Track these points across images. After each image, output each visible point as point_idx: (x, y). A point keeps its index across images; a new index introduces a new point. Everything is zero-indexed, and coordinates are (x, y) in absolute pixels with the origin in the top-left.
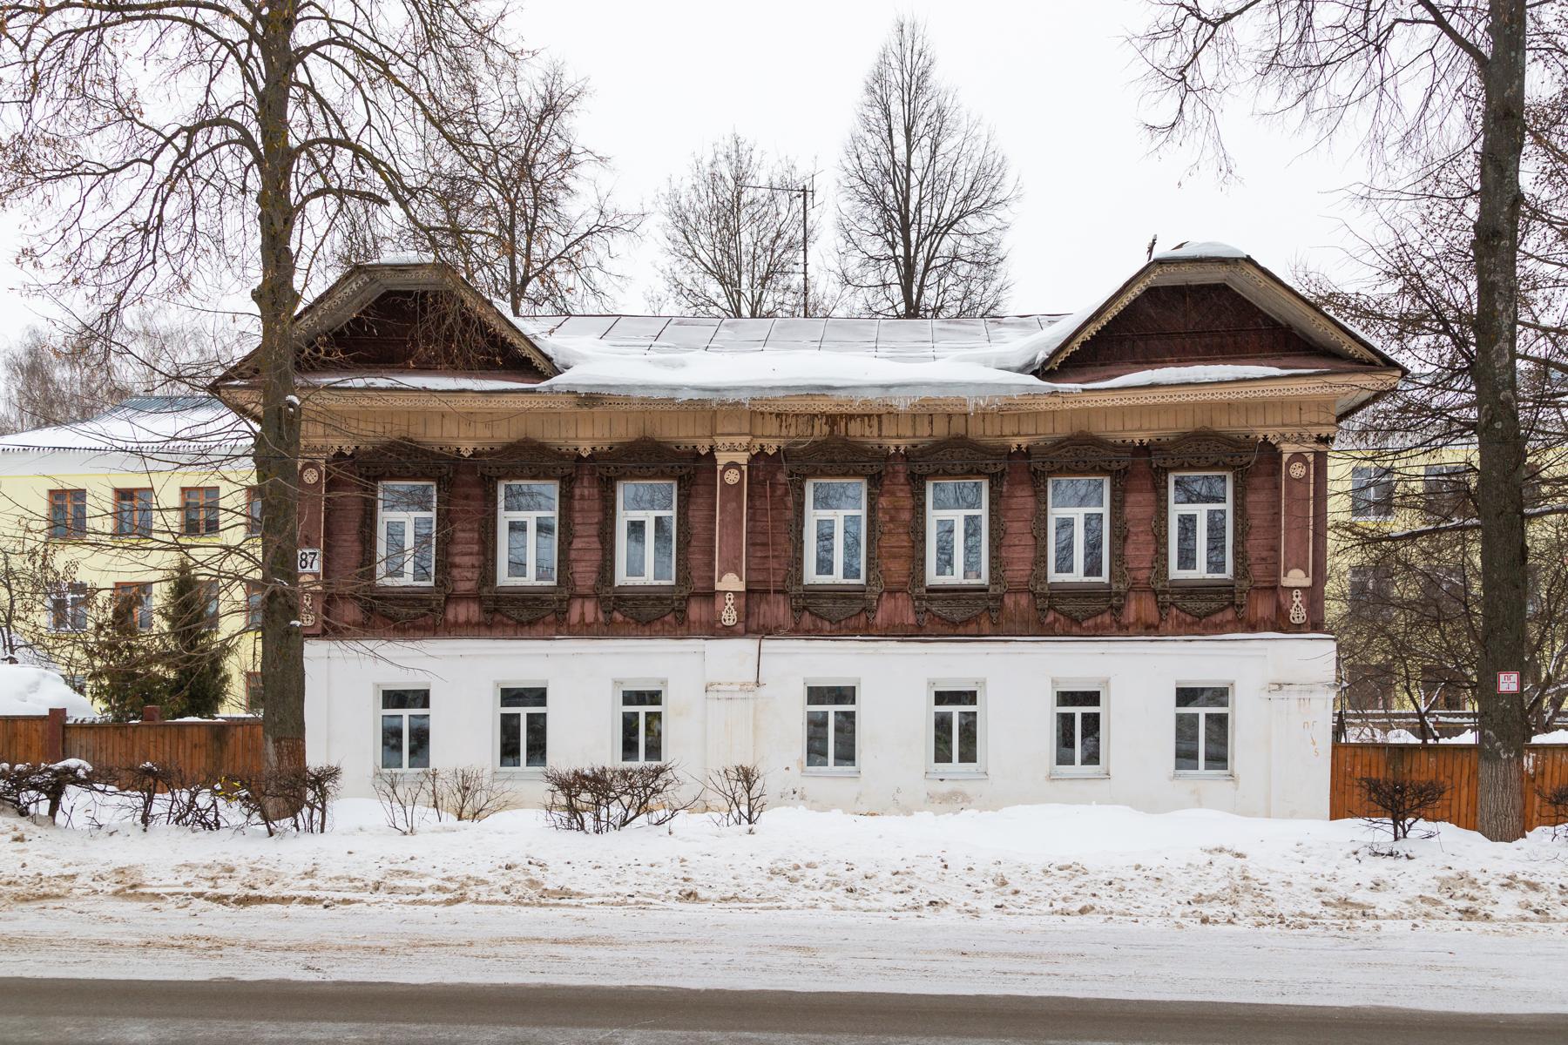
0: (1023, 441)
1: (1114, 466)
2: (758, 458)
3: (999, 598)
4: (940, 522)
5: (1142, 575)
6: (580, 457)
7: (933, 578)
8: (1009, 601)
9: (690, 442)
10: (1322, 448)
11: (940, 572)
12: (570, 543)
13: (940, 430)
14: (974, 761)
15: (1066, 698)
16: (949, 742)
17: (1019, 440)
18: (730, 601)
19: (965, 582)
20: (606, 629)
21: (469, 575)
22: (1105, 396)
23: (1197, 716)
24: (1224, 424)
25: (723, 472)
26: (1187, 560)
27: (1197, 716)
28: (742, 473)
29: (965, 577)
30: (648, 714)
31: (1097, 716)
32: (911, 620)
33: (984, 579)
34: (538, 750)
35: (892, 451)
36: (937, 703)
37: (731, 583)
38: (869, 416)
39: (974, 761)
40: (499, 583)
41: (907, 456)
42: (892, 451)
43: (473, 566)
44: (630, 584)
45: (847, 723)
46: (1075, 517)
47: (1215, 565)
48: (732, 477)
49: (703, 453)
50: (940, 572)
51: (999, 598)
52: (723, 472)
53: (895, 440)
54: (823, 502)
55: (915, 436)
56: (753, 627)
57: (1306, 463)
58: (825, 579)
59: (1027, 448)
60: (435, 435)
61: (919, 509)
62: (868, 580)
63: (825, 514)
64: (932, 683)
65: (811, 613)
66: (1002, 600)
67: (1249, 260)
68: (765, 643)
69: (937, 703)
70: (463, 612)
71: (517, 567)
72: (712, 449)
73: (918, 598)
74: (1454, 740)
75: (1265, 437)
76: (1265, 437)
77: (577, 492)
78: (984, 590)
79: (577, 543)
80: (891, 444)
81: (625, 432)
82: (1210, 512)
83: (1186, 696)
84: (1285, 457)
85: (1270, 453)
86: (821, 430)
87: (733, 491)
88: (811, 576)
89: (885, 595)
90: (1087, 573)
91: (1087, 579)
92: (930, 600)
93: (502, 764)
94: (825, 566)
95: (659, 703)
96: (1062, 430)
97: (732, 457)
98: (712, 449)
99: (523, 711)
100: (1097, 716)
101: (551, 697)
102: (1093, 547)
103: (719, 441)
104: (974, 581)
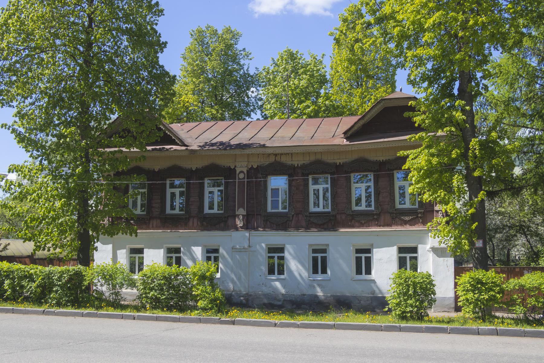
0: (341, 161)
3: (335, 216)
6: (193, 170)
7: (312, 209)
8: (338, 217)
9: (228, 165)
11: (357, 205)
12: (189, 199)
13: (313, 158)
14: (313, 273)
15: (358, 251)
19: (324, 210)
21: (157, 210)
23: (361, 257)
25: (238, 175)
26: (317, 204)
27: (361, 257)
28: (245, 174)
29: (324, 208)
33: (329, 209)
35: (296, 166)
36: (269, 253)
37: (241, 212)
38: (288, 154)
39: (313, 273)
40: (167, 213)
42: (296, 166)
43: (158, 207)
44: (209, 212)
45: (324, 260)
46: (406, 184)
47: (369, 205)
49: (232, 167)
50: (357, 205)
51: (335, 216)
52: (238, 175)
53: (297, 162)
54: (316, 182)
55: (346, 159)
56: (247, 226)
58: (212, 211)
59: (343, 164)
60: (373, 157)
61: (307, 185)
62: (289, 210)
63: (316, 187)
64: (310, 245)
65: (270, 222)
66: (336, 216)
69: (269, 253)
71: (173, 208)
72: (235, 167)
73: (306, 216)
74: (235, 279)
78: (329, 213)
79: (192, 199)
80: (296, 163)
81: (205, 163)
83: (272, 250)
84: (237, 172)
86: (272, 159)
89: (295, 215)
90: (366, 207)
91: (366, 209)
92: (310, 217)
94: (211, 207)
98: (235, 167)
102: (368, 197)
104: (326, 210)
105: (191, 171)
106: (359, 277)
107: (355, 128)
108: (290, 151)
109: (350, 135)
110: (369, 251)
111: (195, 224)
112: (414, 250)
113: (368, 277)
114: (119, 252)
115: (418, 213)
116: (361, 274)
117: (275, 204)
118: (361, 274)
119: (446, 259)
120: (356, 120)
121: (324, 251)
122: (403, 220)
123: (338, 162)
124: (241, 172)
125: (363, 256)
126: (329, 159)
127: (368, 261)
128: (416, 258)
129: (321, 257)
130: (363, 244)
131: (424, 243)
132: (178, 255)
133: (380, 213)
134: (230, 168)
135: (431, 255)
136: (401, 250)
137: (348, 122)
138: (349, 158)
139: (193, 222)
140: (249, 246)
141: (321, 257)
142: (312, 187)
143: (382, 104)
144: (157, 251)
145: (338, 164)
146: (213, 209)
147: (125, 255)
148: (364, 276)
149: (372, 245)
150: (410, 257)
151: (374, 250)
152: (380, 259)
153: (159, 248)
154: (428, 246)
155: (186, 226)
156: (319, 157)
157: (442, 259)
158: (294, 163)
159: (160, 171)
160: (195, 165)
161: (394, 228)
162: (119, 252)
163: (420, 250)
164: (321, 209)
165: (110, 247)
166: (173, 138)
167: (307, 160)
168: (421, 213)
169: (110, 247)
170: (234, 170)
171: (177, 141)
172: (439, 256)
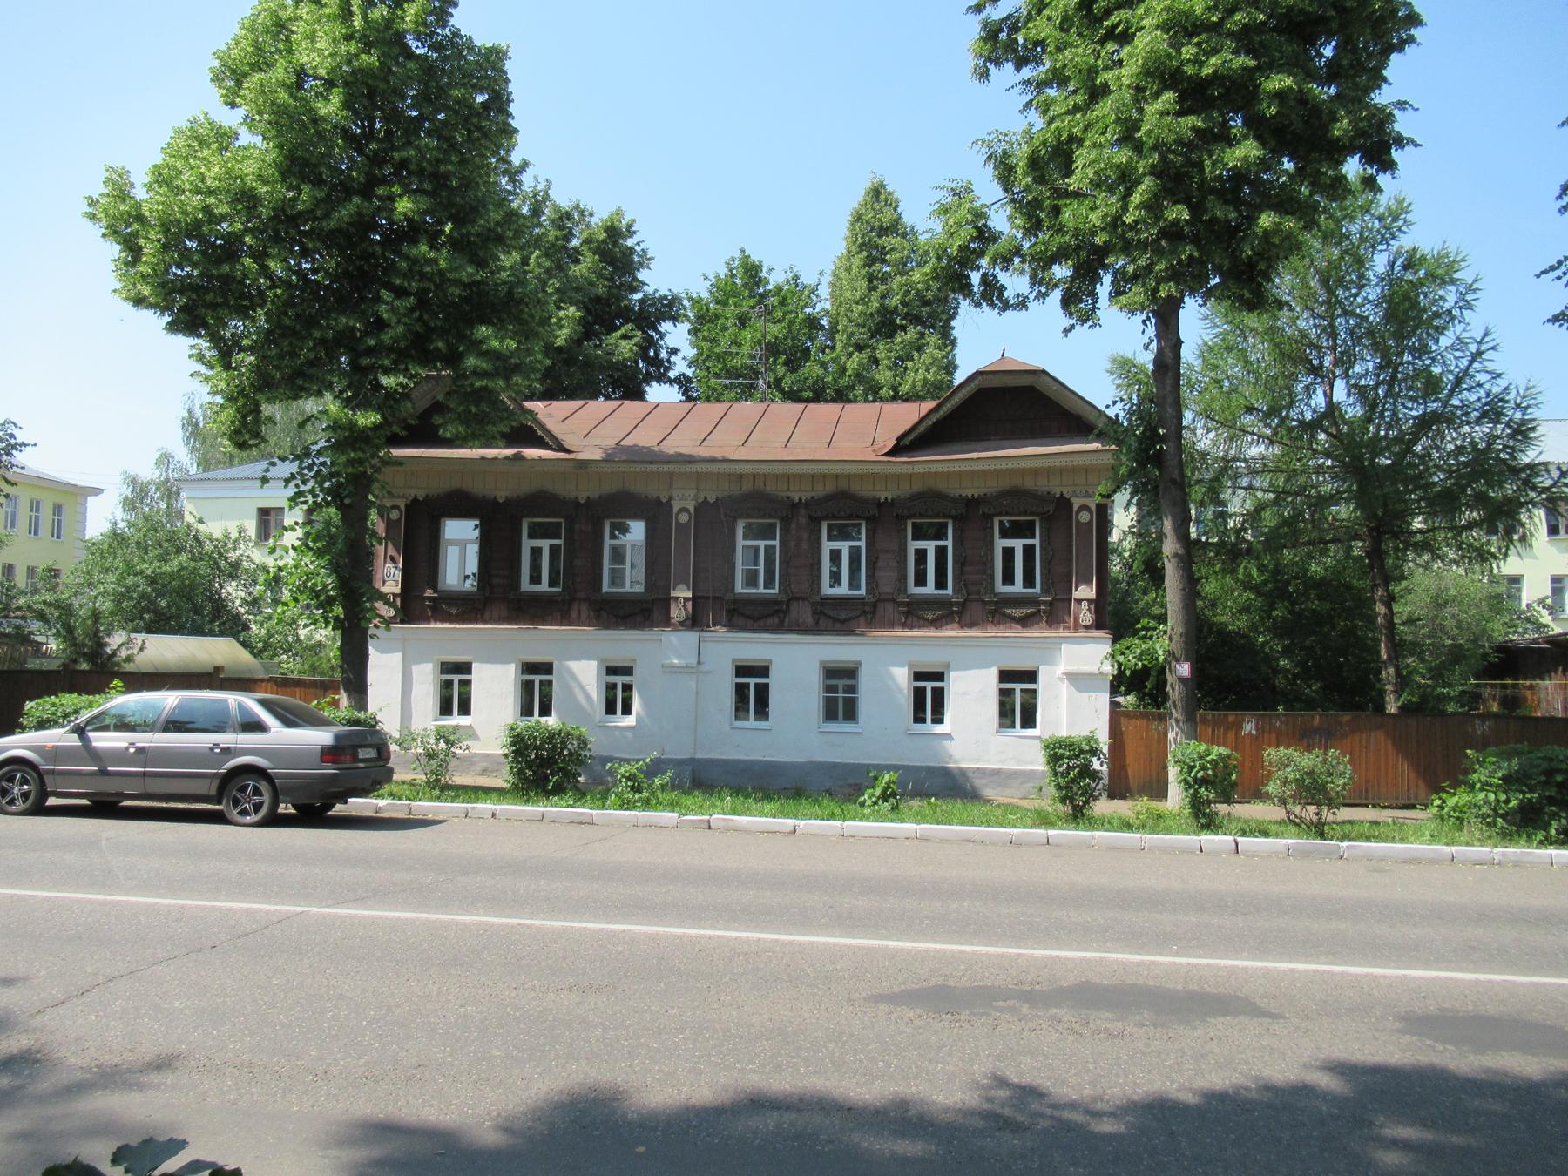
1: (953, 512)
2: (702, 507)
4: (832, 551)
5: (888, 589)
6: (498, 503)
10: (1105, 501)
11: (613, 583)
15: (919, 676)
16: (924, 710)
17: (799, 494)
18: (1084, 607)
20: (815, 629)
22: (906, 466)
23: (925, 688)
24: (1029, 484)
25: (677, 514)
27: (925, 688)
30: (541, 682)
31: (942, 689)
32: (811, 620)
33: (863, 591)
34: (1029, 720)
36: (738, 675)
37: (683, 593)
41: (807, 505)
45: (762, 692)
48: (683, 518)
49: (664, 500)
52: (677, 514)
56: (695, 622)
57: (1091, 512)
60: (479, 488)
64: (734, 660)
67: (1044, 372)
68: (703, 634)
69: (738, 675)
70: (888, 610)
75: (1062, 494)
76: (1062, 494)
77: (577, 527)
82: (1024, 545)
83: (742, 670)
84: (1075, 507)
85: (1064, 504)
87: (683, 528)
88: (526, 585)
92: (822, 605)
93: (737, 718)
95: (767, 675)
96: (917, 487)
97: (684, 503)
98: (670, 498)
99: (752, 681)
100: (767, 686)
101: (772, 672)
103: (675, 493)
105: (880, 505)
106: (920, 727)
107: (922, 429)
108: (788, 473)
109: (904, 446)
110: (939, 676)
111: (584, 615)
112: (1031, 676)
113: (939, 729)
114: (416, 669)
115: (1040, 603)
116: (923, 721)
117: (617, 578)
118: (923, 721)
119: (1094, 694)
120: (923, 413)
121: (763, 671)
122: (835, 620)
123: (882, 496)
124: (1084, 508)
125: (929, 685)
126: (867, 491)
127: (939, 696)
128: (468, 683)
129: (756, 685)
130: (929, 658)
131: (1051, 662)
132: (850, 682)
133: (966, 600)
134: (658, 502)
135: (1064, 688)
136: (1006, 676)
137: (905, 416)
138: (904, 490)
139: (579, 614)
140: (699, 663)
141: (756, 685)
142: (827, 546)
143: (976, 382)
144: (499, 667)
145: (882, 500)
146: (1013, 583)
147: (431, 677)
148: (930, 727)
149: (948, 666)
150: (460, 681)
151: (952, 674)
152: (965, 694)
153: (504, 661)
154: (1060, 669)
155: (565, 618)
156: (843, 485)
157: (1086, 695)
158: (792, 495)
159: (508, 501)
160: (584, 491)
161: (432, 626)
162: (416, 669)
163: (1041, 678)
164: (843, 590)
165: (397, 657)
166: (540, 433)
167: (820, 490)
168: (1045, 602)
169: (397, 657)
170: (669, 505)
171: (547, 439)
172: (1079, 690)
